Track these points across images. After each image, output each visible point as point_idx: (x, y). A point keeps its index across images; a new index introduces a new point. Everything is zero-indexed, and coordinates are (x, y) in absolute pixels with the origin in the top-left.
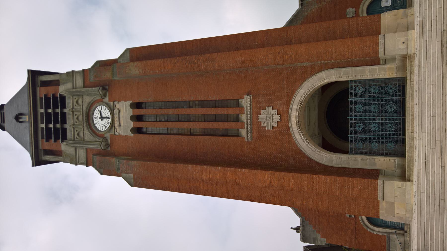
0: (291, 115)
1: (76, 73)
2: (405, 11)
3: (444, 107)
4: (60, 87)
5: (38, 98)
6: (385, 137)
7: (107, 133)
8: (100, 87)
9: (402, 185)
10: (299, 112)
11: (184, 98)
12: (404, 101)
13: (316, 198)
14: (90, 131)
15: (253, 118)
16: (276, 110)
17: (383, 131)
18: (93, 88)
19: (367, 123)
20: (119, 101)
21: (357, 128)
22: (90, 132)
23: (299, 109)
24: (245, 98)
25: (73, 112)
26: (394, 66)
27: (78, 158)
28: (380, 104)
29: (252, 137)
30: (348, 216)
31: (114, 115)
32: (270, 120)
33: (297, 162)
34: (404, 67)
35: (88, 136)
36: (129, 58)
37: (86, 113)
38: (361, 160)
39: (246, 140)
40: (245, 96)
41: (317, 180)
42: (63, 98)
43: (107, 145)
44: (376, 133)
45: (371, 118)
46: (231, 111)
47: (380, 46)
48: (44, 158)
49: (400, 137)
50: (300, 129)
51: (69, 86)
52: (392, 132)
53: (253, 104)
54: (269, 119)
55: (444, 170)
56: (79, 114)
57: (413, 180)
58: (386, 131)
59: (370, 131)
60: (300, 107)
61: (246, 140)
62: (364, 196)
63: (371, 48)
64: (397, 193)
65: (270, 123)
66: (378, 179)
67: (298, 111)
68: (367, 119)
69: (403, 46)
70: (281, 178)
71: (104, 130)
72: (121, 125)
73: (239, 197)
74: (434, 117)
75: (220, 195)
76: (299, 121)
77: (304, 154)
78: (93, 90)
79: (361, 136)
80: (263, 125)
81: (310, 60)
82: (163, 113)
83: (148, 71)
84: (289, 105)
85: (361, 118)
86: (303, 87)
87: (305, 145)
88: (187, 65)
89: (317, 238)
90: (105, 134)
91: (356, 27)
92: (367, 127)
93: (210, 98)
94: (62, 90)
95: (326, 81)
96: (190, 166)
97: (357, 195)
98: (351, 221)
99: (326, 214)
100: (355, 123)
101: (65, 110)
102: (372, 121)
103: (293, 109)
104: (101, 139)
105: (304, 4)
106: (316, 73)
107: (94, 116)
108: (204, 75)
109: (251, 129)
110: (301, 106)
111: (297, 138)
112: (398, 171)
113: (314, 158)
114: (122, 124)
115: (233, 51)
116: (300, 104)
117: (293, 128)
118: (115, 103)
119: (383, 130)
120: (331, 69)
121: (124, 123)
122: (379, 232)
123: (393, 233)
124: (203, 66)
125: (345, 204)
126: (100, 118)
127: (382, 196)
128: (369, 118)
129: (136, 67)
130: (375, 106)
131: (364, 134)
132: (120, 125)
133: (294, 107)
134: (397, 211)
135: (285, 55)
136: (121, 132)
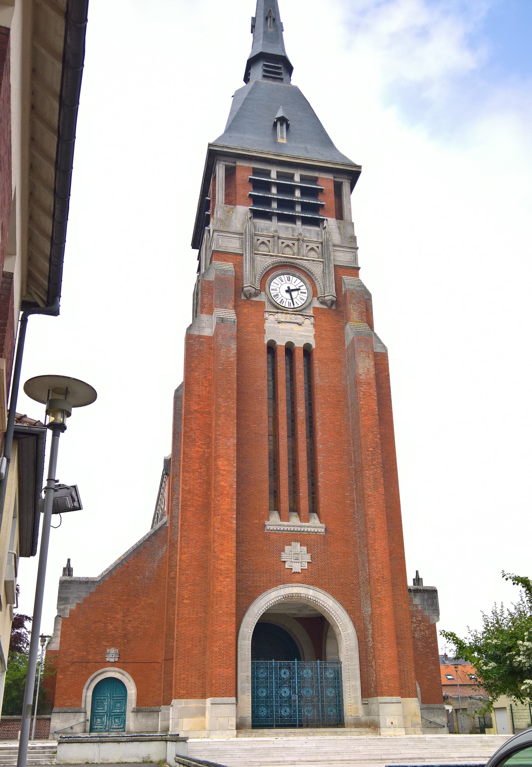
0: (301, 587)
1: (354, 253)
2: (419, 724)
3: (353, 762)
5: (316, 174)
6: (274, 704)
7: (267, 297)
8: (335, 297)
9: (231, 725)
10: (304, 598)
11: (320, 434)
12: (270, 727)
13: (193, 618)
14: (270, 268)
15: (295, 534)
16: (306, 568)
17: (281, 702)
18: (334, 285)
19: (289, 683)
20: (315, 325)
21: (283, 671)
23: (308, 598)
24: (321, 525)
26: (360, 713)
28: (313, 698)
29: (270, 531)
30: (107, 652)
31: (295, 314)
32: (295, 559)
33: (240, 593)
34: (358, 724)
37: (296, 264)
38: (248, 676)
39: (267, 523)
40: (323, 525)
41: (230, 622)
42: (317, 222)
43: (249, 296)
44: (278, 694)
45: (297, 687)
46: (304, 502)
47: (389, 697)
48: (221, 165)
49: (274, 722)
50: (283, 598)
51: (336, 238)
52: (280, 712)
53: (314, 535)
54: (296, 557)
55: (291, 765)
57: (239, 737)
58: (280, 705)
59: (280, 686)
60: (310, 599)
61: (267, 523)
62: (214, 681)
63: (387, 688)
64: (221, 720)
65: (289, 559)
67: (306, 596)
68: (294, 682)
69: (388, 723)
70: (227, 574)
72: (280, 324)
73: (185, 508)
74: (337, 754)
75: (186, 479)
76: (293, 597)
77: (251, 603)
79: (274, 675)
80: (287, 548)
81: (375, 616)
82: (299, 397)
84: (312, 585)
85: (296, 675)
86: (335, 604)
87: (263, 604)
88: (370, 449)
89: (69, 604)
90: (266, 293)
91: (404, 670)
92: (285, 683)
93: (321, 474)
94: (331, 222)
95: (342, 633)
97: (214, 672)
98: (100, 656)
99: (108, 619)
100: (290, 668)
102: (292, 689)
103: (308, 589)
104: (258, 286)
105: (411, 593)
106: (353, 621)
107: (291, 277)
108: (350, 467)
109: (282, 531)
110: (312, 601)
111: (272, 594)
113: (246, 616)
114: (281, 326)
115: (386, 517)
116: (314, 599)
117: (284, 589)
119: (282, 702)
120: (357, 641)
121: (283, 329)
122: (86, 696)
123: (85, 717)
124: (369, 473)
125: (188, 656)
126: (288, 287)
127: (216, 702)
128: (295, 686)
129: (368, 369)
130: (310, 692)
131: (276, 679)
133: (311, 591)
134: (185, 720)
135: (381, 586)
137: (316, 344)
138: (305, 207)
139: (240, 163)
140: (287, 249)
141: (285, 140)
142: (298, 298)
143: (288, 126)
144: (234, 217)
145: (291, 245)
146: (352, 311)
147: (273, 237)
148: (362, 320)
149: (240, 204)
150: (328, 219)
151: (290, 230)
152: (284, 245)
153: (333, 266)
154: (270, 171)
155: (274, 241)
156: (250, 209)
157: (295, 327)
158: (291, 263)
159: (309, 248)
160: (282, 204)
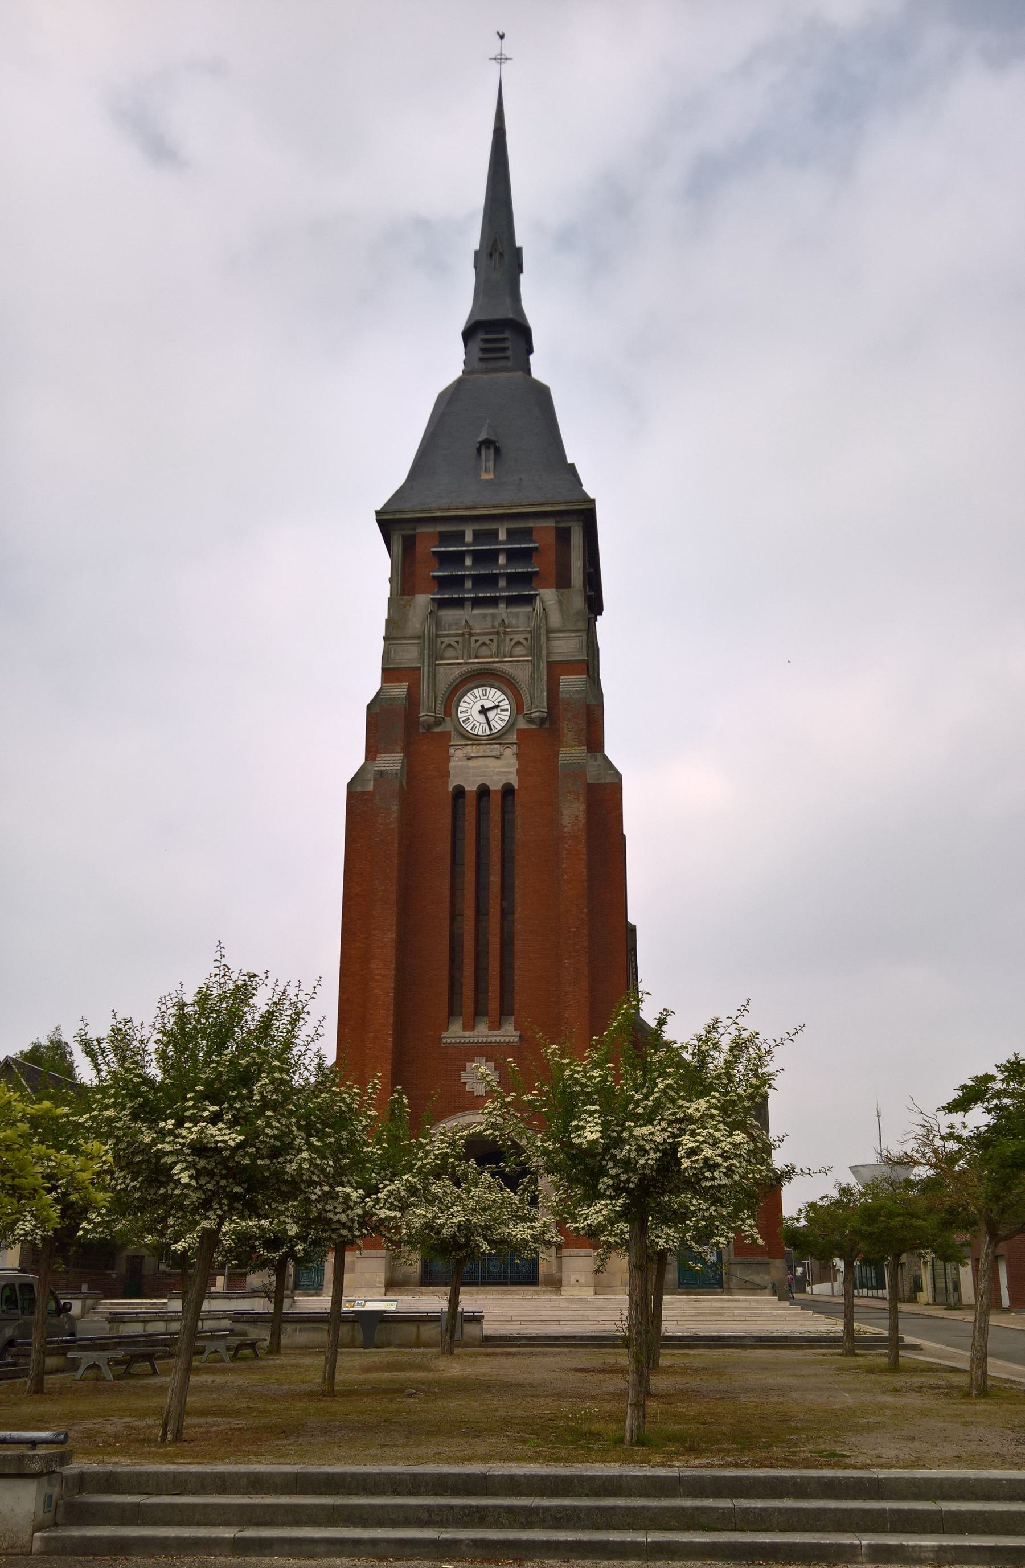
4: (554, 590)
5: (530, 524)
9: (380, 1282)
11: (519, 909)
20: (518, 756)
22: (454, 681)
24: (515, 1033)
25: (498, 633)
27: (397, 642)
35: (449, 672)
36: (603, 781)
42: (529, 600)
56: (494, 647)
64: (368, 1276)
66: (531, 558)
71: (460, 715)
78: (542, 693)
83: (567, 846)
90: (452, 720)
96: (394, 935)
101: (502, 606)
107: (488, 689)
112: (399, 1276)
114: (471, 763)
118: (515, 746)
121: (474, 768)
126: (482, 706)
132: (470, 758)
136: (457, 761)
137: (520, 781)
138: (513, 579)
139: (422, 530)
140: (484, 648)
141: (492, 473)
142: (496, 719)
143: (497, 451)
144: (411, 613)
145: (488, 642)
146: (566, 731)
147: (463, 634)
148: (579, 742)
149: (420, 593)
150: (541, 591)
151: (489, 619)
152: (479, 643)
153: (545, 665)
154: (464, 531)
155: (464, 641)
156: (433, 599)
157: (492, 763)
158: (487, 669)
159: (513, 642)
160: (479, 581)
